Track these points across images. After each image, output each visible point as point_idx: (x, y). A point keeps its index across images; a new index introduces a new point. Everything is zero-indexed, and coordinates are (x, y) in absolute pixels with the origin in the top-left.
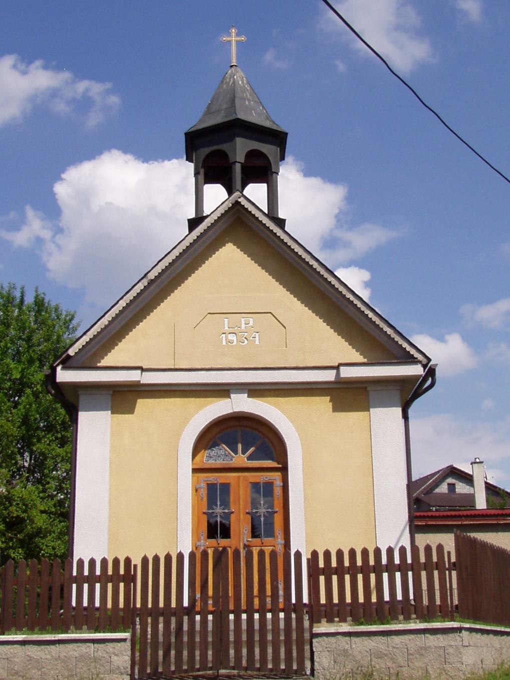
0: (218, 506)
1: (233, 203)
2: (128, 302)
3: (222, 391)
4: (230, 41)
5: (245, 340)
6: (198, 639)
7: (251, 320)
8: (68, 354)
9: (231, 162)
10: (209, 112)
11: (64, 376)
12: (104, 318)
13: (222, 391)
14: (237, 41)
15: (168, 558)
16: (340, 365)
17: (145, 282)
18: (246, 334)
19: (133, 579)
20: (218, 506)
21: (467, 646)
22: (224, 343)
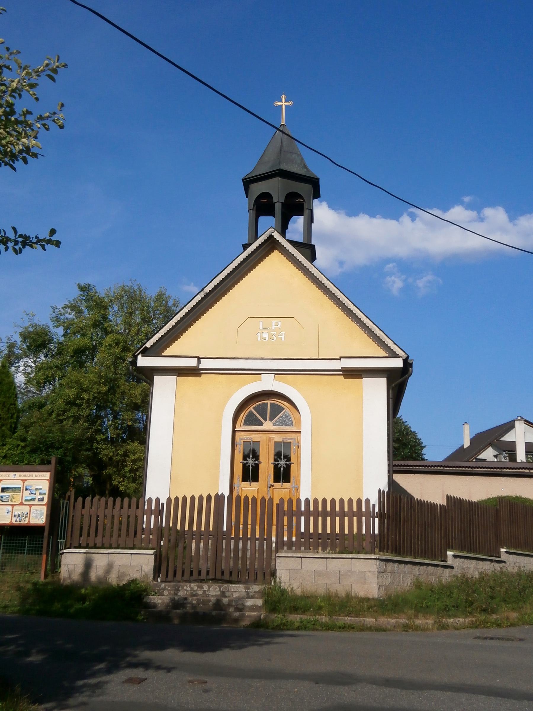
0: (251, 459)
1: (268, 236)
2: (190, 309)
3: (257, 372)
4: (280, 106)
5: (274, 337)
6: (240, 555)
7: (280, 323)
8: (146, 347)
9: (274, 202)
10: (260, 162)
11: (143, 361)
12: (171, 321)
13: (257, 372)
14: (286, 106)
15: (201, 498)
16: (341, 358)
17: (202, 295)
18: (275, 333)
19: (161, 512)
20: (251, 459)
21: (383, 572)
22: (259, 340)
